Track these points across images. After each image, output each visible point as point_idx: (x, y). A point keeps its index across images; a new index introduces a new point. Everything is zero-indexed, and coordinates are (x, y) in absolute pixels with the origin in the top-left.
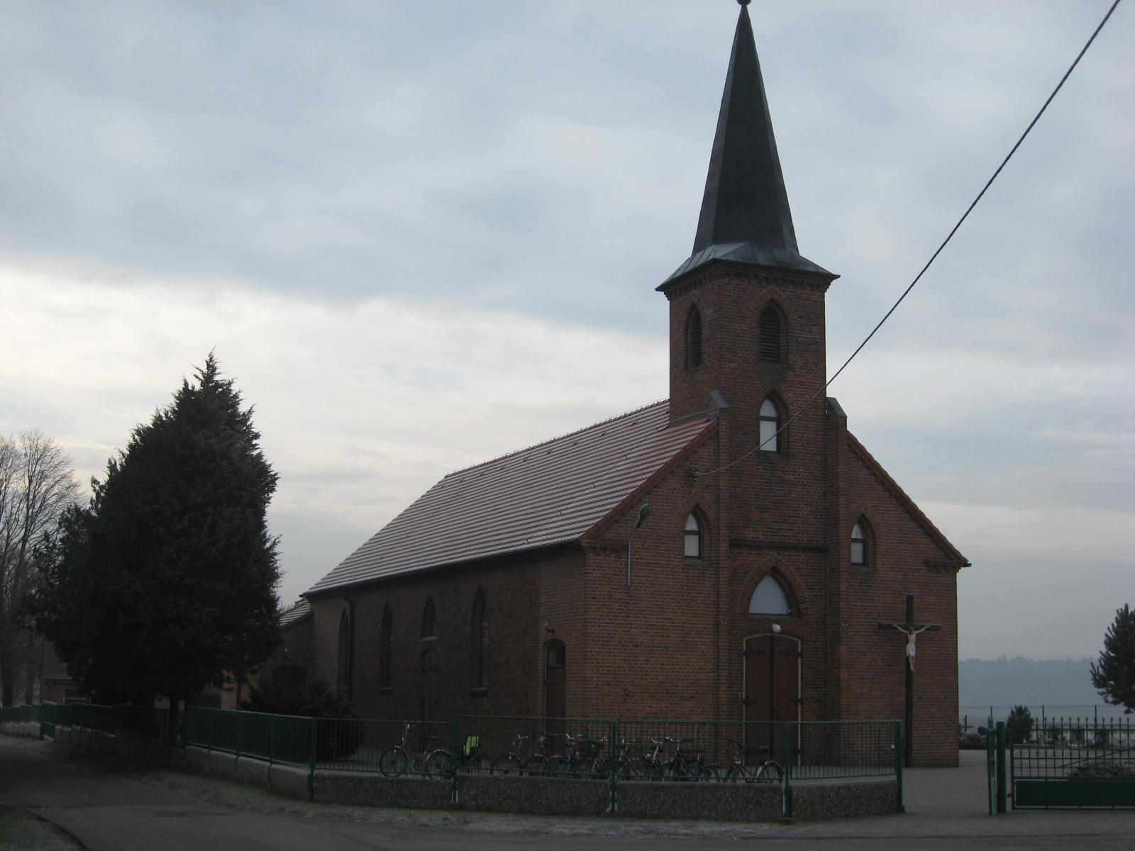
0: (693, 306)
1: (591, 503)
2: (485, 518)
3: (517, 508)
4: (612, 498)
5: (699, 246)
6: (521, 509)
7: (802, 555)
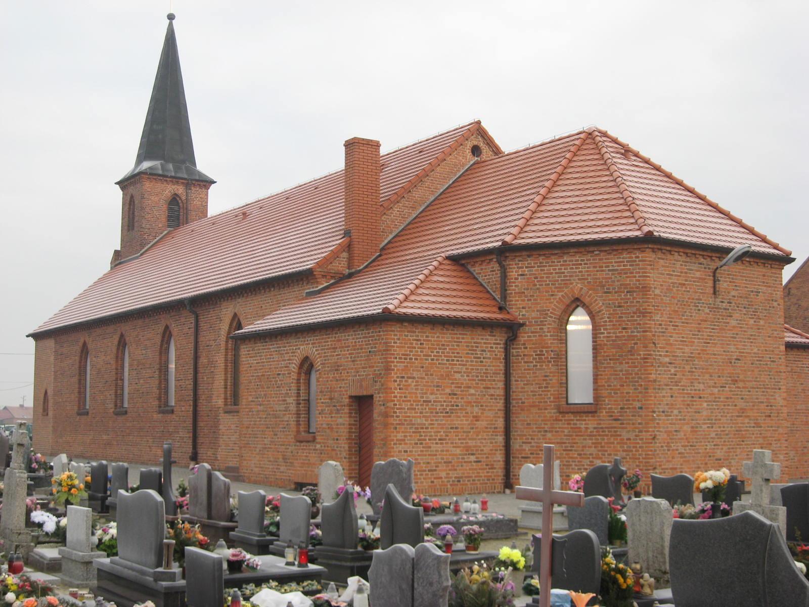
5: (140, 159)
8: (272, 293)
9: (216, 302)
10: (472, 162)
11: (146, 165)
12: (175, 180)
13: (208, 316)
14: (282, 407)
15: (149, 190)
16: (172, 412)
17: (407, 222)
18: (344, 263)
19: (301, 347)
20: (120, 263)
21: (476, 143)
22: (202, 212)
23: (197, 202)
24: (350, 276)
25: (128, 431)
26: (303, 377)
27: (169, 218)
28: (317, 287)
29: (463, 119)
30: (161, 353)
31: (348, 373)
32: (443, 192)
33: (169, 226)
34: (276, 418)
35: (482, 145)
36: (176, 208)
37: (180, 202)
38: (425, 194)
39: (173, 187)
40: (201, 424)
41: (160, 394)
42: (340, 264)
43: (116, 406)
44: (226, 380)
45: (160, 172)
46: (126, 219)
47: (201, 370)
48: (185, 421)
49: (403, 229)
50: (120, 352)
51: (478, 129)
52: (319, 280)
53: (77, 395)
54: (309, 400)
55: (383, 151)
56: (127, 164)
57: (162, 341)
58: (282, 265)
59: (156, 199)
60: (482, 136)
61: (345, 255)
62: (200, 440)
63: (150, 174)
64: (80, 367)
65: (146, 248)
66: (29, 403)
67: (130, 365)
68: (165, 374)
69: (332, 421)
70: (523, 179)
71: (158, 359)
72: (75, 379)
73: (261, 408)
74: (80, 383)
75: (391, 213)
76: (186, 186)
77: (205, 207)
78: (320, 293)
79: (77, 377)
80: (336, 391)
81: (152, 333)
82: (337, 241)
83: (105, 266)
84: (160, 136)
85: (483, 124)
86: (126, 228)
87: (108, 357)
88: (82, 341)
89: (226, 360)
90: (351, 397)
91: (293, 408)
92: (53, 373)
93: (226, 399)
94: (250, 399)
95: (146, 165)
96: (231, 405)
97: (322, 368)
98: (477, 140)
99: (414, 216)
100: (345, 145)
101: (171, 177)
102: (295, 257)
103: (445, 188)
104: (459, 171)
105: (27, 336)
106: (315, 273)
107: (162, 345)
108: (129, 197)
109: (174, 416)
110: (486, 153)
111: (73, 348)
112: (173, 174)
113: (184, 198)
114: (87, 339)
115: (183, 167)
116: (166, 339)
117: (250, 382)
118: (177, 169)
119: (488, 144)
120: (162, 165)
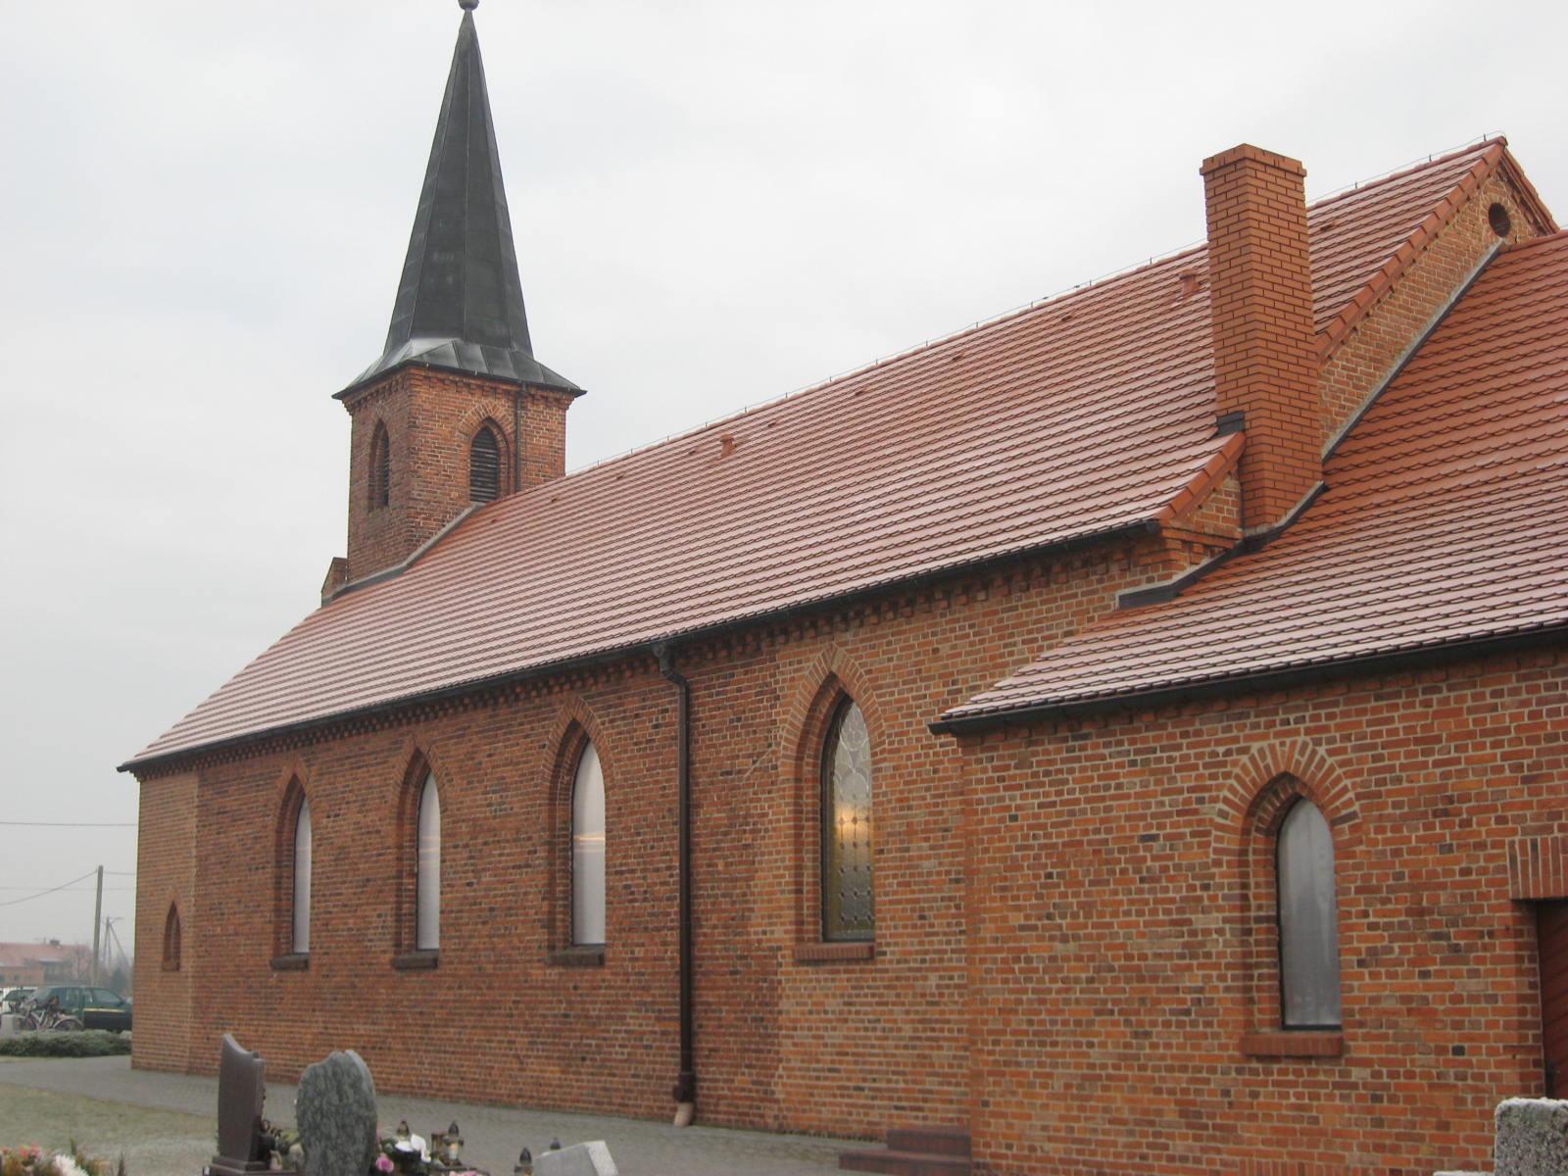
0: (381, 424)
1: (398, 673)
2: (361, 686)
3: (490, 632)
4: (398, 673)
5: (398, 335)
6: (552, 619)
7: (1444, 686)
8: (979, 608)
9: (758, 650)
10: (1493, 249)
11: (417, 347)
12: (490, 383)
13: (724, 693)
14: (1174, 945)
15: (427, 406)
16: (600, 961)
17: (1367, 402)
18: (1231, 511)
19: (1255, 747)
21: (1496, 198)
22: (551, 465)
23: (539, 441)
24: (1252, 546)
25: (439, 1014)
26: (1258, 841)
27: (475, 477)
28: (1169, 576)
29: (1452, 134)
30: (552, 799)
31: (1501, 820)
32: (1438, 324)
33: (474, 498)
34: (1141, 979)
35: (1510, 205)
37: (499, 438)
38: (1403, 327)
39: (484, 401)
40: (705, 996)
41: (551, 912)
42: (1220, 510)
43: (398, 945)
44: (798, 868)
45: (455, 364)
46: (364, 483)
47: (703, 840)
48: (646, 989)
49: (1360, 419)
50: (409, 800)
51: (1498, 165)
52: (1173, 556)
53: (269, 915)
54: (1278, 919)
55: (1315, 191)
56: (366, 353)
57: (558, 766)
59: (445, 429)
60: (1511, 183)
61: (1231, 484)
62: (704, 1043)
63: (430, 369)
64: (279, 844)
65: (420, 550)
67: (446, 835)
68: (566, 857)
69: (1428, 988)
71: (544, 816)
72: (266, 876)
73: (1072, 947)
75: (1331, 373)
76: (515, 402)
77: (561, 452)
78: (1179, 595)
79: (270, 870)
80: (1443, 886)
81: (524, 746)
82: (1204, 452)
83: (315, 603)
84: (450, 280)
85: (1511, 148)
86: (364, 503)
87: (372, 816)
88: (286, 774)
89: (798, 812)
90: (1518, 903)
91: (1223, 945)
92: (193, 862)
93: (799, 923)
94: (1017, 919)
95: (417, 347)
96: (816, 940)
97: (1363, 808)
98: (337, 562)
99: (1382, 385)
100: (1204, 172)
101: (481, 376)
103: (1441, 312)
104: (1466, 269)
105: (121, 769)
106: (1165, 533)
107: (555, 776)
108: (370, 429)
110: (1521, 228)
111: (254, 797)
112: (485, 370)
113: (509, 429)
114: (302, 771)
115: (507, 353)
116: (567, 760)
117: (1016, 867)
118: (491, 358)
119: (1523, 203)
120: (455, 346)
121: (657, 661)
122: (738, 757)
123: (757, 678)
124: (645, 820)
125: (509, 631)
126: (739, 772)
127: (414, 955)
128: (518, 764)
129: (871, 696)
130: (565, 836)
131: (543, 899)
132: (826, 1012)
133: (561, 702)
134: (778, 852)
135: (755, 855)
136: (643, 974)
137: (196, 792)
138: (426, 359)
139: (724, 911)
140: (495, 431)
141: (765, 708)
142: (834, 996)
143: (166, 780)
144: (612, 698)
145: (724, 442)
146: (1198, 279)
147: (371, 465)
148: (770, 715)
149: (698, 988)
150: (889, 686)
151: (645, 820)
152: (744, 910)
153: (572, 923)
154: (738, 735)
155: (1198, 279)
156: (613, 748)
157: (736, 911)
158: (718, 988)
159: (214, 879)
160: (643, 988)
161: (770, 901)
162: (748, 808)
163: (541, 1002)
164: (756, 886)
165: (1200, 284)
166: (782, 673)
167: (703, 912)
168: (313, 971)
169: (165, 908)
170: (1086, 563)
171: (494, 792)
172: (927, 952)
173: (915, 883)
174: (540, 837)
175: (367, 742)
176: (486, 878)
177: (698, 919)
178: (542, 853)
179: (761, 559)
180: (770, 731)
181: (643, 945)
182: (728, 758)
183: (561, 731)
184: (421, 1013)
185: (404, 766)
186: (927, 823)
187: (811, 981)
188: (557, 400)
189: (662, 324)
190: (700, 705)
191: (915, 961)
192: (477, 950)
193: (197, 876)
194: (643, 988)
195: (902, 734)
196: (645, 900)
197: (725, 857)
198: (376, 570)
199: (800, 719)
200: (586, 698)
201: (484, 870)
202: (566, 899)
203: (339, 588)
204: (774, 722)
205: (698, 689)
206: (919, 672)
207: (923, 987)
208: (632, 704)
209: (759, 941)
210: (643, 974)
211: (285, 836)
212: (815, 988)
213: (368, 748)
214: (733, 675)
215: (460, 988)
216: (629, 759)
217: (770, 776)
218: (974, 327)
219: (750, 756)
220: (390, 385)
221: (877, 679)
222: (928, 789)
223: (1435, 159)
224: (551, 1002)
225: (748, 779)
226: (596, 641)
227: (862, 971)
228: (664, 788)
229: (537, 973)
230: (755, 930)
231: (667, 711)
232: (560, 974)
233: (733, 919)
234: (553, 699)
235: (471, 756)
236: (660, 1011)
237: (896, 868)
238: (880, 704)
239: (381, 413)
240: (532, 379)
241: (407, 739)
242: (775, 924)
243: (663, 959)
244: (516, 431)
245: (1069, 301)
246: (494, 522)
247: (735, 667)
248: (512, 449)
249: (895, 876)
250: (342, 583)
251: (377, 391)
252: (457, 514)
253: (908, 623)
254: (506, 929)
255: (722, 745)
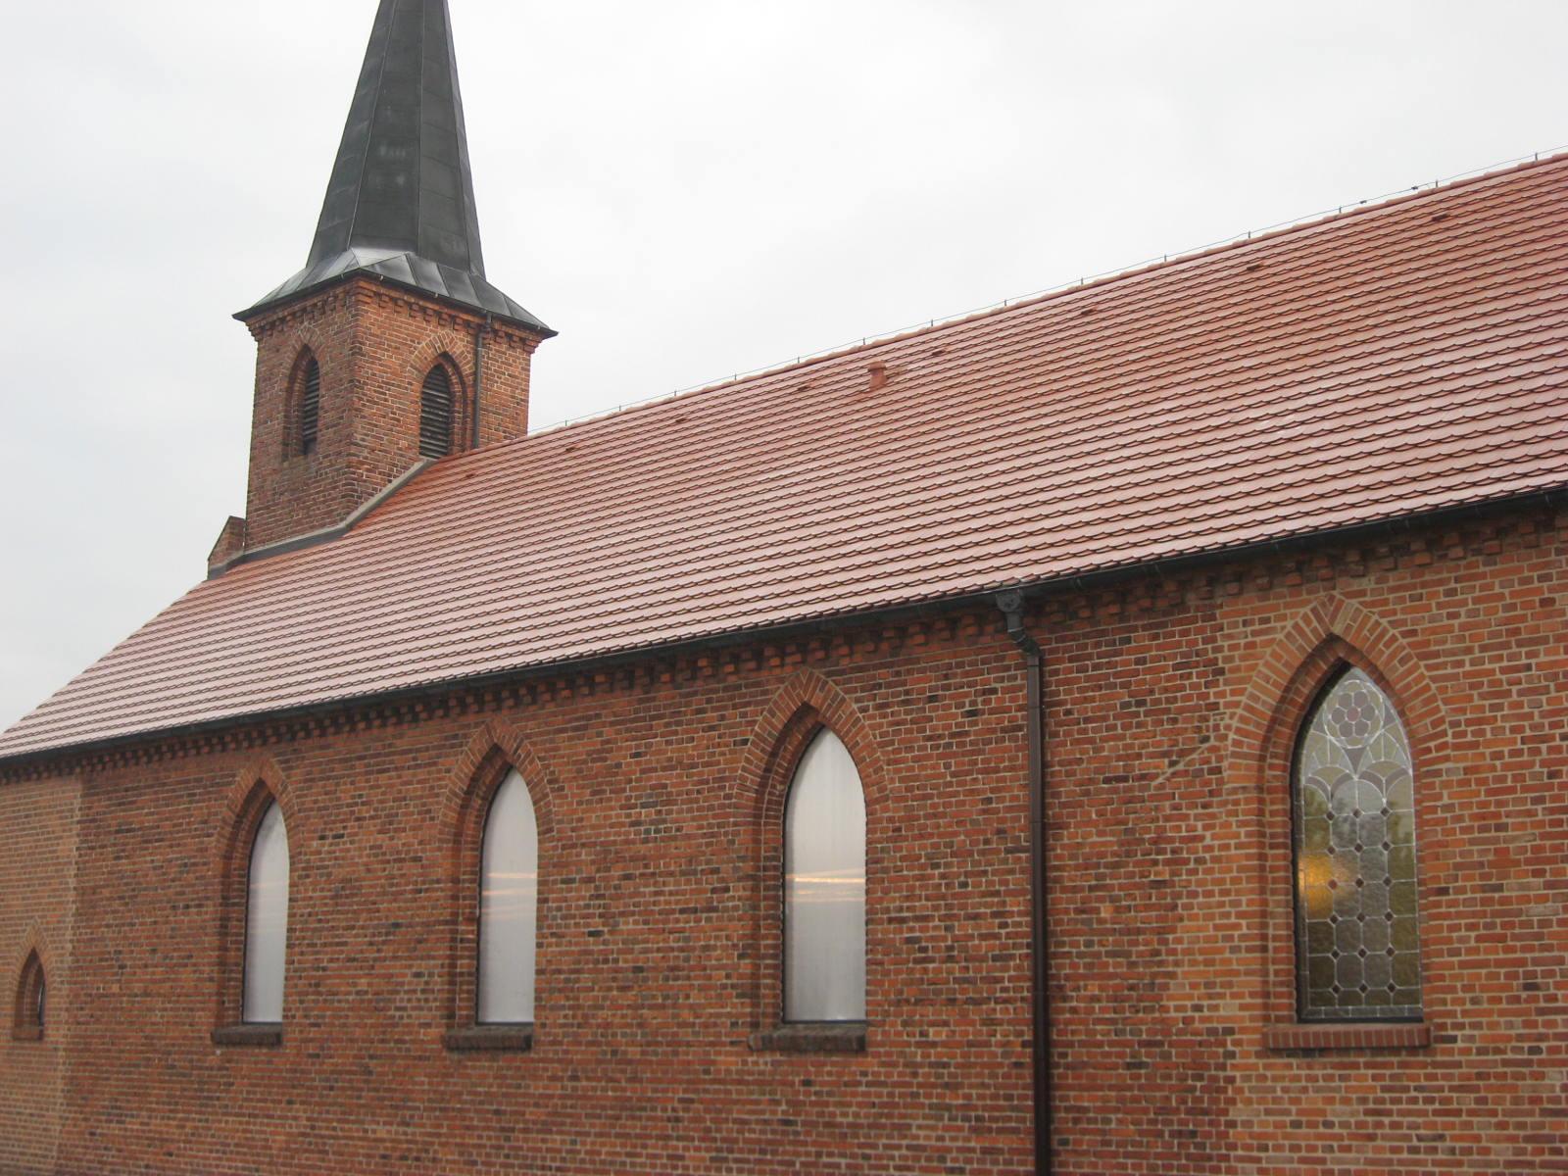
5: (327, 243)
12: (449, 310)
15: (374, 330)
20: (244, 560)
33: (423, 451)
36: (441, 397)
37: (454, 379)
39: (441, 332)
45: (411, 281)
46: (277, 425)
50: (471, 818)
56: (282, 259)
58: (170, 683)
59: (395, 361)
64: (226, 875)
65: (362, 509)
66: (260, 1019)
70: (415, 576)
74: (223, 929)
76: (476, 337)
83: (200, 573)
86: (276, 449)
92: (71, 896)
95: (365, 257)
98: (233, 522)
102: (243, 659)
108: (288, 358)
109: (871, 1064)
112: (445, 292)
113: (467, 369)
118: (451, 279)
121: (1003, 616)
122: (1139, 756)
123: (1179, 644)
124: (950, 845)
125: (162, 676)
126: (1143, 777)
127: (474, 1031)
128: (693, 766)
129: (1416, 667)
130: (775, 868)
131: (741, 956)
132: (1328, 1124)
133: (781, 680)
134: (1225, 893)
135: (1179, 896)
136: (945, 1065)
137: (77, 803)
138: (378, 270)
139: (1111, 976)
140: (450, 370)
141: (1194, 686)
142: (1346, 1101)
143: (25, 786)
144: (884, 675)
145: (876, 371)
146: (886, 373)
147: (288, 400)
148: (1206, 696)
149: (1059, 1087)
150: (1453, 653)
151: (950, 845)
152: (1154, 975)
153: (783, 991)
154: (1139, 725)
155: (886, 373)
156: (882, 745)
157: (1141, 976)
158: (1101, 1088)
159: (109, 919)
160: (946, 1086)
161: (1209, 963)
162: (1161, 830)
163: (736, 1102)
164: (1179, 941)
165: (888, 377)
166: (1230, 637)
167: (1067, 977)
168: (289, 1049)
169: (19, 956)
170: (1499, 533)
171: (643, 806)
172: (1542, 1038)
173: (1515, 937)
174: (736, 869)
175: (401, 736)
176: (627, 925)
177: (1061, 988)
178: (739, 891)
179: (392, 633)
180: (1206, 719)
181: (945, 1024)
182: (1119, 758)
183: (780, 720)
184: (497, 1112)
185: (469, 770)
186: (1536, 849)
187: (1297, 1078)
188: (523, 340)
189: (641, 266)
190: (1059, 683)
191: (1515, 1050)
192: (608, 1025)
193: (78, 914)
194: (946, 1086)
195: (1480, 721)
196: (951, 959)
197: (1113, 899)
198: (294, 533)
199: (1268, 700)
200: (829, 674)
201: (622, 914)
202: (774, 957)
203: (235, 555)
204: (1214, 706)
205: (1059, 661)
206: (1516, 632)
207: (1534, 1089)
208: (922, 683)
209: (1187, 1021)
210: (945, 1065)
211: (235, 864)
212: (1305, 1090)
213: (402, 744)
214: (1128, 640)
215: (575, 1078)
216: (916, 759)
217: (1208, 783)
218: (617, 410)
219: (1164, 754)
220: (325, 302)
221: (1427, 643)
222: (1537, 801)
223: (937, 324)
224: (757, 1102)
225: (1162, 786)
226: (182, 715)
227: (1403, 1065)
228: (989, 800)
229: (728, 1061)
230: (1178, 1001)
231: (994, 691)
232: (773, 1063)
233: (1132, 988)
234: (764, 676)
235: (599, 756)
236: (978, 1119)
237: (1474, 914)
238: (1434, 679)
239: (306, 337)
240: (497, 310)
241: (476, 732)
242: (1221, 996)
243: (987, 1044)
244: (475, 374)
245: (909, 342)
246: (469, 477)
247: (1135, 629)
248: (470, 394)
249: (1471, 927)
250: (238, 549)
251: (304, 310)
252: (406, 468)
253: (1485, 564)
254: (666, 997)
255: (1104, 740)
